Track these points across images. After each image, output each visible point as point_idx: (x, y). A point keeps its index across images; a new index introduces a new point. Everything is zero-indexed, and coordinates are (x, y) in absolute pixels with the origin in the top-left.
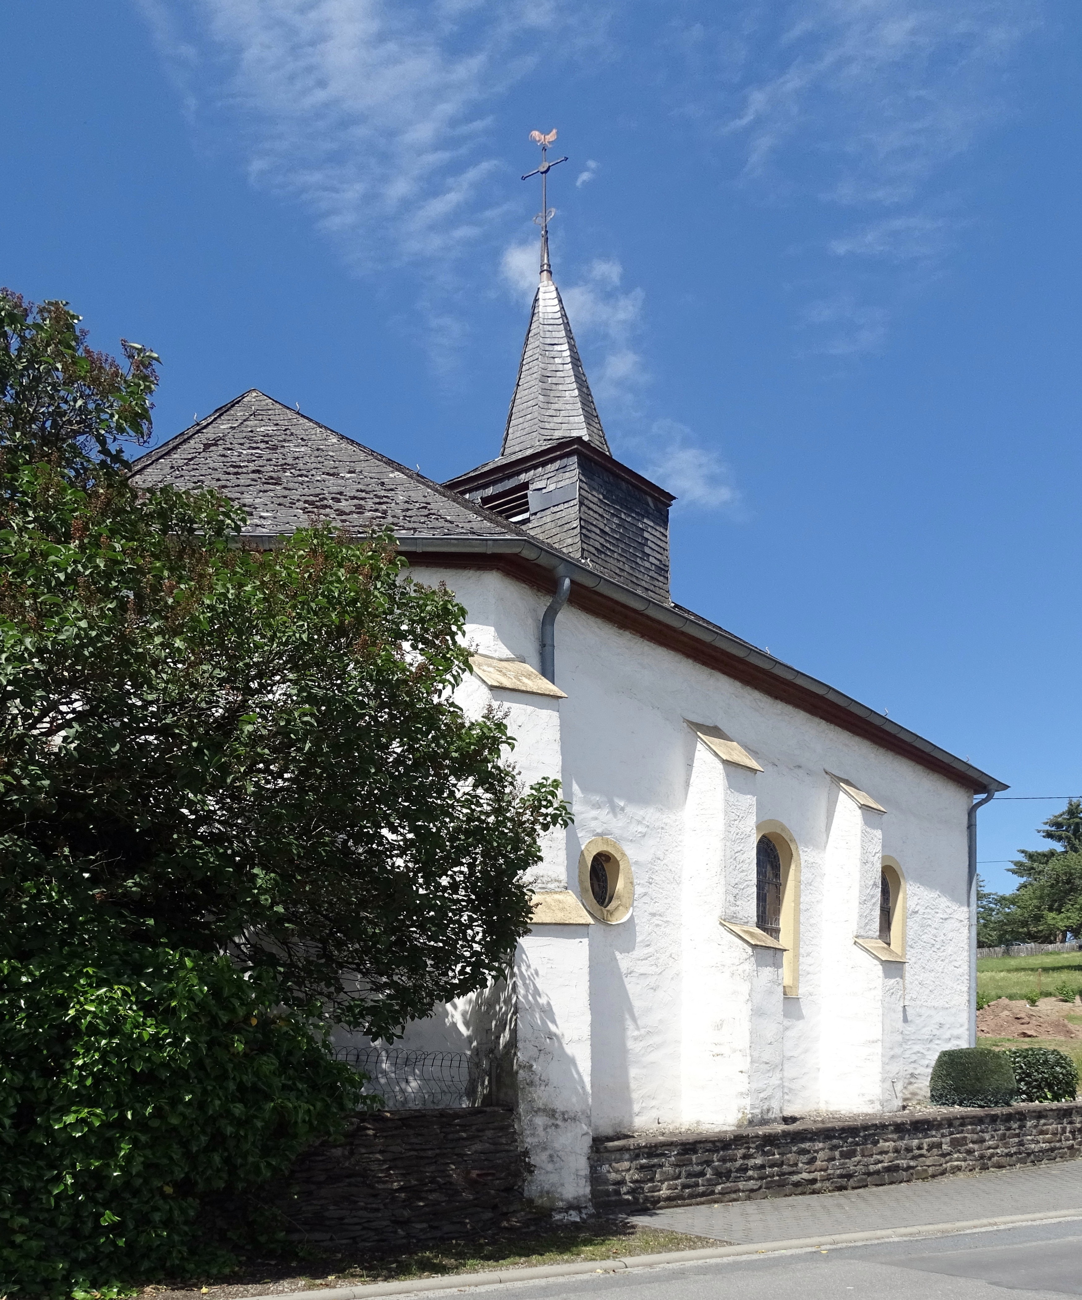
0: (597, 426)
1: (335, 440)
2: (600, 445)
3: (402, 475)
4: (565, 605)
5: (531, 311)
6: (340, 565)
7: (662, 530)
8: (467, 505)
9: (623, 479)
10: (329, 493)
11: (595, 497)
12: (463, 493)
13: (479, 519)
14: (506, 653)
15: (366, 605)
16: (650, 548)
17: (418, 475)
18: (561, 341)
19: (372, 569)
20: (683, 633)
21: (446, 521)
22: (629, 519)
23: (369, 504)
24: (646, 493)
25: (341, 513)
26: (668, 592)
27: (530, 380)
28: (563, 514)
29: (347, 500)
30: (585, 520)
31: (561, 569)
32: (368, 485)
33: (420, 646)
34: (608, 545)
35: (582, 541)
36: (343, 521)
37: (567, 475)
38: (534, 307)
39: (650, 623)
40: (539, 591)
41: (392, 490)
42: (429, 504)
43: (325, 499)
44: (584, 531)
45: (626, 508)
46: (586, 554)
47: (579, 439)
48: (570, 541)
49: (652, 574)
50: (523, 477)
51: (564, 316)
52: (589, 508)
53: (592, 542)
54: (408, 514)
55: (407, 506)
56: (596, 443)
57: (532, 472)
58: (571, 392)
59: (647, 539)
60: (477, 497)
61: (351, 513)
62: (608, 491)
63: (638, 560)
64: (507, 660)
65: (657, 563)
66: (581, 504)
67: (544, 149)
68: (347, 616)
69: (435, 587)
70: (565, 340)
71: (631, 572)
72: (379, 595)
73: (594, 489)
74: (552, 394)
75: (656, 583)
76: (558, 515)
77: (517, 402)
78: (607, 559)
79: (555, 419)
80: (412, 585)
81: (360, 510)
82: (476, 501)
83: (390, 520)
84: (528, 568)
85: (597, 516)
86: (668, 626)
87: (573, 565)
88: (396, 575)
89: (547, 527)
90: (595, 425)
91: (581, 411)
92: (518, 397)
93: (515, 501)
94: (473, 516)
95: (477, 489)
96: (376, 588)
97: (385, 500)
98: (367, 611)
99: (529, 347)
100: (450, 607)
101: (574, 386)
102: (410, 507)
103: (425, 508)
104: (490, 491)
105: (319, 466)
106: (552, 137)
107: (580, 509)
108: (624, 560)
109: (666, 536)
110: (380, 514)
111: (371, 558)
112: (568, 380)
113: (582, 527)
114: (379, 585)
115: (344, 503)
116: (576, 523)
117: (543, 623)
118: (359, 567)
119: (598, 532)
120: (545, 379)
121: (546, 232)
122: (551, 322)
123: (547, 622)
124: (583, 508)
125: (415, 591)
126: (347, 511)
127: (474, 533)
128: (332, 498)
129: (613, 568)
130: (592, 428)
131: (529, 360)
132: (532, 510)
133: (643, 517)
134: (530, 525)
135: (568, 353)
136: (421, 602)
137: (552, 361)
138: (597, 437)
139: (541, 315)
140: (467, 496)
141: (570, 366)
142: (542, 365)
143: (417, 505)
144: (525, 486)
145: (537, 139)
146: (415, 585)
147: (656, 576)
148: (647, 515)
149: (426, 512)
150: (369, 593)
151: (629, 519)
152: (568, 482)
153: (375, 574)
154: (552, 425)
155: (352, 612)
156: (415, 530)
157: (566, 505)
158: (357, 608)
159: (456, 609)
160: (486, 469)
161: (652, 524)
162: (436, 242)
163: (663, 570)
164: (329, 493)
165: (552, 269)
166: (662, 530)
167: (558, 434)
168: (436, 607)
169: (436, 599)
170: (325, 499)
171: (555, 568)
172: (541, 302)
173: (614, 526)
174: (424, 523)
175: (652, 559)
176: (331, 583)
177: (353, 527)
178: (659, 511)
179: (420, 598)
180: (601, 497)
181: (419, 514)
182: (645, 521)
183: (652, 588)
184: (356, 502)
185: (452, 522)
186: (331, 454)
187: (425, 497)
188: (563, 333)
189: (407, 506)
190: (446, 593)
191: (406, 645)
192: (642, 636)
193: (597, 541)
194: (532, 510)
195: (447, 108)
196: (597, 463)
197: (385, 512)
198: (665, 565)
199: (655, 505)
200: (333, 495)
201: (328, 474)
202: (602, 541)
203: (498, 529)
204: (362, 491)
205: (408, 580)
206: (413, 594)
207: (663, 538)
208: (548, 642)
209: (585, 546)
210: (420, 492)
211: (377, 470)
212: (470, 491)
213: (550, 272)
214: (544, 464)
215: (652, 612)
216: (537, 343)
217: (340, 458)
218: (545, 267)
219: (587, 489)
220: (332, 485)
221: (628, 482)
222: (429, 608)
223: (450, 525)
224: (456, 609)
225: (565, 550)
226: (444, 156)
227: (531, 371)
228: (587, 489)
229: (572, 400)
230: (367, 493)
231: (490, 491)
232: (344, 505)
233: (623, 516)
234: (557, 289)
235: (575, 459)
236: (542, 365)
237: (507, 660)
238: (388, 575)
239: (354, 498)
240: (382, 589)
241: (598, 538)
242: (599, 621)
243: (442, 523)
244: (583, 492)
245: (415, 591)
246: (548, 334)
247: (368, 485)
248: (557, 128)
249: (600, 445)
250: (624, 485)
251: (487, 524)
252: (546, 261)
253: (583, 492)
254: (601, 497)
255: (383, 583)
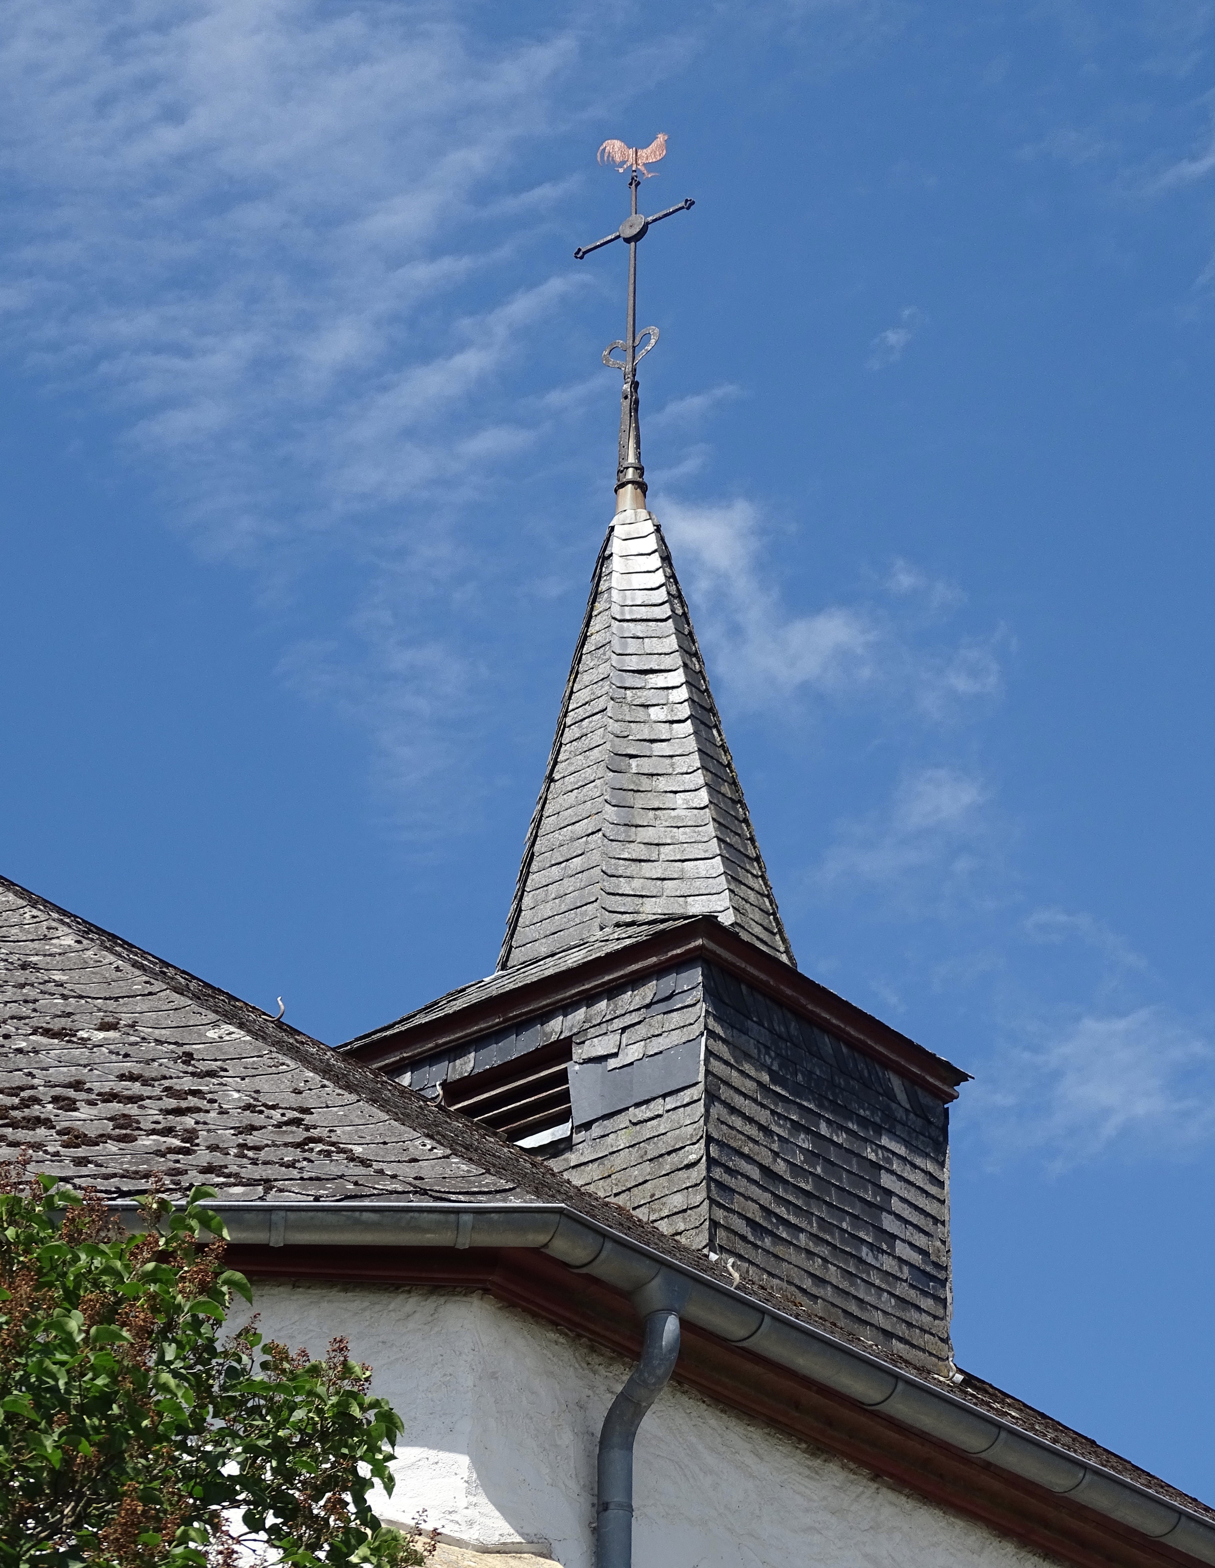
0: (758, 884)
1: (69, 941)
2: (764, 935)
3: (239, 1034)
4: (665, 1392)
5: (590, 586)
6: (72, 1299)
7: (930, 1167)
8: (405, 1109)
9: (826, 1028)
10: (48, 1084)
11: (749, 1078)
12: (396, 1070)
13: (439, 1152)
14: (498, 1528)
15: (134, 1413)
16: (899, 1217)
17: (279, 1024)
18: (667, 662)
19: (155, 1310)
20: (987, 1466)
21: (352, 1159)
22: (840, 1138)
23: (150, 1114)
24: (887, 1064)
25: (75, 1138)
26: (945, 1341)
27: (581, 764)
28: (662, 1126)
29: (91, 1103)
30: (720, 1143)
31: (656, 1290)
32: (147, 1062)
33: (271, 1519)
34: (782, 1211)
35: (712, 1201)
36: (81, 1162)
37: (676, 1018)
39: (894, 1436)
40: (593, 1349)
41: (211, 1074)
42: (307, 1111)
43: (36, 1100)
44: (718, 1173)
45: (835, 1107)
46: (722, 1236)
47: (709, 922)
48: (678, 1201)
49: (901, 1289)
50: (558, 1027)
51: (677, 597)
52: (733, 1110)
53: (738, 1203)
54: (252, 1139)
55: (250, 1118)
56: (754, 932)
57: (581, 1014)
58: (689, 794)
59: (889, 1193)
60: (432, 1081)
61: (103, 1138)
62: (785, 1062)
63: (865, 1253)
64: (502, 1550)
65: (916, 1258)
66: (711, 1097)
67: (635, 182)
68: (85, 1443)
69: (319, 1356)
70: (676, 660)
71: (844, 1285)
72: (173, 1383)
73: (747, 1056)
74: (640, 801)
75: (913, 1316)
76: (648, 1130)
77: (548, 824)
78: (780, 1250)
79: (647, 870)
80: (257, 1350)
81: (125, 1129)
82: (429, 1093)
83: (203, 1157)
84: (566, 1287)
85: (752, 1131)
86: (945, 1447)
87: (690, 1279)
88: (218, 1323)
89: (618, 1161)
90: (751, 881)
91: (714, 847)
92: (549, 809)
93: (534, 1092)
94: (421, 1145)
95: (433, 1058)
96: (161, 1361)
97: (192, 1101)
98: (137, 1427)
99: (585, 678)
100: (356, 1411)
101: (699, 778)
102: (258, 1120)
103: (297, 1122)
104: (466, 1065)
105: (25, 1010)
106: (653, 153)
107: (707, 1111)
108: (824, 1251)
109: (941, 1184)
110: (177, 1142)
111: (150, 1278)
112: (682, 764)
113: (712, 1162)
114: (170, 1352)
115: (85, 1112)
116: (695, 1152)
117: (604, 1442)
118: (119, 1302)
119: (756, 1174)
120: (623, 763)
121: (635, 385)
122: (643, 613)
123: (612, 1442)
124: (717, 1110)
125: (264, 1366)
126: (92, 1134)
127: (424, 1192)
128: (55, 1100)
129: (795, 1273)
130: (742, 891)
131: (581, 713)
132: (579, 1117)
133: (879, 1130)
134: (573, 1158)
135: (683, 693)
136: (280, 1398)
137: (641, 714)
138: (758, 915)
139: (615, 595)
140: (406, 1079)
141: (688, 727)
142: (615, 727)
143: (276, 1115)
144: (561, 1050)
145: (618, 158)
146: (266, 1350)
147: (912, 1295)
148: (888, 1124)
149: (300, 1134)
150: (139, 1373)
151: (840, 1138)
152: (677, 1038)
153: (160, 1321)
154: (637, 884)
155: (96, 1430)
156: (268, 1184)
157: (671, 1102)
158: (111, 1419)
159: (371, 1415)
160: (460, 1004)
161: (902, 1150)
163: (931, 1278)
164: (48, 1084)
165: (646, 478)
166: (930, 1167)
167: (651, 909)
168: (320, 1412)
169: (321, 1390)
170: (36, 1100)
171: (640, 1285)
172: (616, 564)
173: (799, 1159)
174: (291, 1165)
175: (901, 1249)
176: (47, 1350)
177: (107, 1177)
178: (921, 1112)
179: (280, 1387)
180: (765, 1078)
181: (280, 1140)
182: (885, 1141)
183: (902, 1330)
184: (116, 1107)
185: (365, 1163)
186: (58, 976)
187: (299, 1092)
188: (672, 643)
189: (250, 1118)
190: (347, 1370)
191: (234, 1519)
192: (877, 1476)
193: (754, 1199)
194: (579, 1117)
196: (755, 985)
197: (190, 1136)
198: (936, 1265)
199: (912, 1097)
200: (58, 1091)
201: (47, 1032)
202: (765, 1198)
203: (489, 1179)
204: (132, 1078)
205: (248, 1335)
206: (259, 1376)
207: (933, 1190)
208: (616, 1497)
209: (720, 1215)
210: (286, 1079)
211: (175, 1019)
212: (414, 1064)
213: (642, 487)
214: (612, 991)
215: (902, 1408)
217: (79, 989)
218: (630, 474)
219: (727, 1056)
220: (56, 1062)
221: (838, 1035)
222: (299, 1414)
223: (362, 1170)
224: (371, 1415)
225: (664, 1227)
227: (585, 743)
228: (727, 1056)
229: (690, 817)
230: (146, 1082)
231: (466, 1065)
232: (86, 1117)
233: (824, 1129)
235: (696, 975)
236: (615, 727)
237: (502, 1550)
238: (196, 1324)
239: (110, 1097)
240: (178, 1364)
241: (755, 1191)
242: (757, 1434)
243: (338, 1166)
244: (717, 1067)
245: (264, 1366)
246: (632, 646)
247: (147, 1062)
249: (764, 935)
250: (827, 1043)
251: (460, 1166)
252: (631, 459)
253: (717, 1067)
254: (765, 1078)
255: (180, 1346)
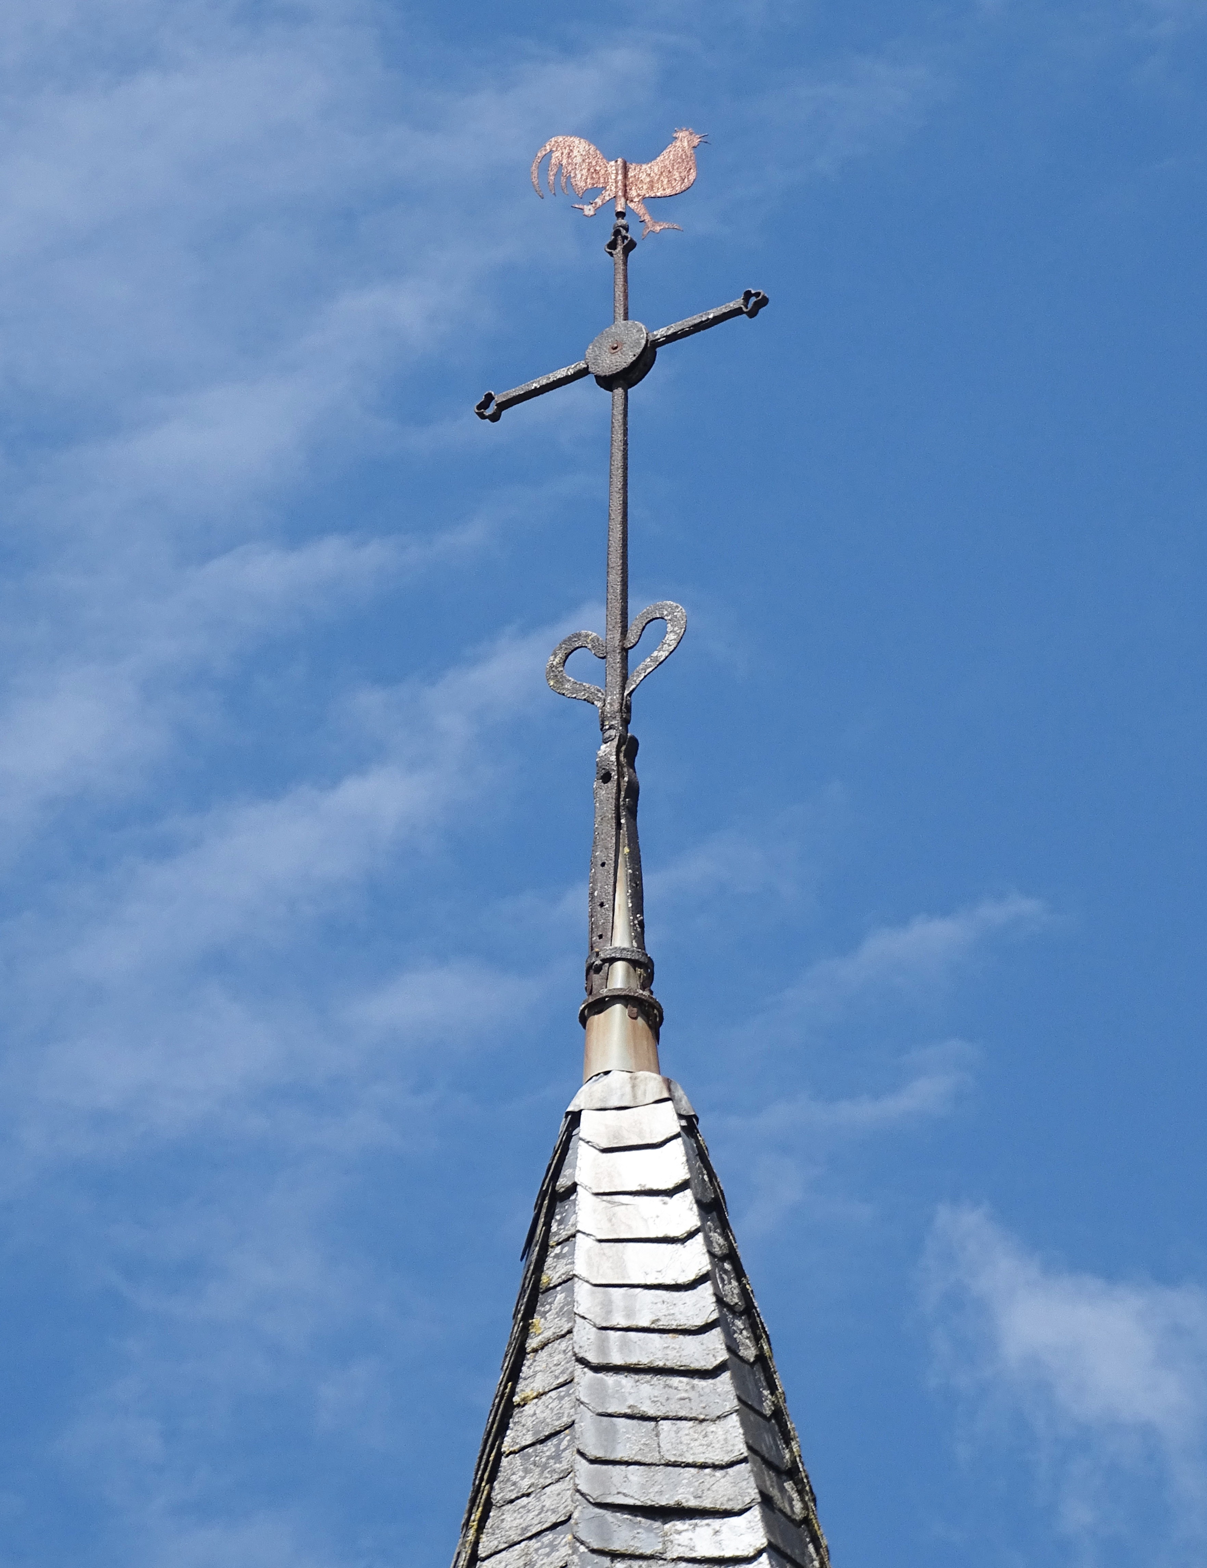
38: (539, 1245)
51: (739, 1312)
67: (622, 242)
70: (740, 1485)
121: (629, 748)
139: (585, 1299)
145: (581, 179)
162: (233, 1051)
165: (660, 992)
172: (586, 1214)
188: (729, 1437)
195: (406, 309)
213: (647, 1011)
216: (556, 1500)
218: (619, 977)
226: (342, 564)
234: (690, 1127)
246: (630, 1440)
248: (694, 125)
252: (621, 938)
